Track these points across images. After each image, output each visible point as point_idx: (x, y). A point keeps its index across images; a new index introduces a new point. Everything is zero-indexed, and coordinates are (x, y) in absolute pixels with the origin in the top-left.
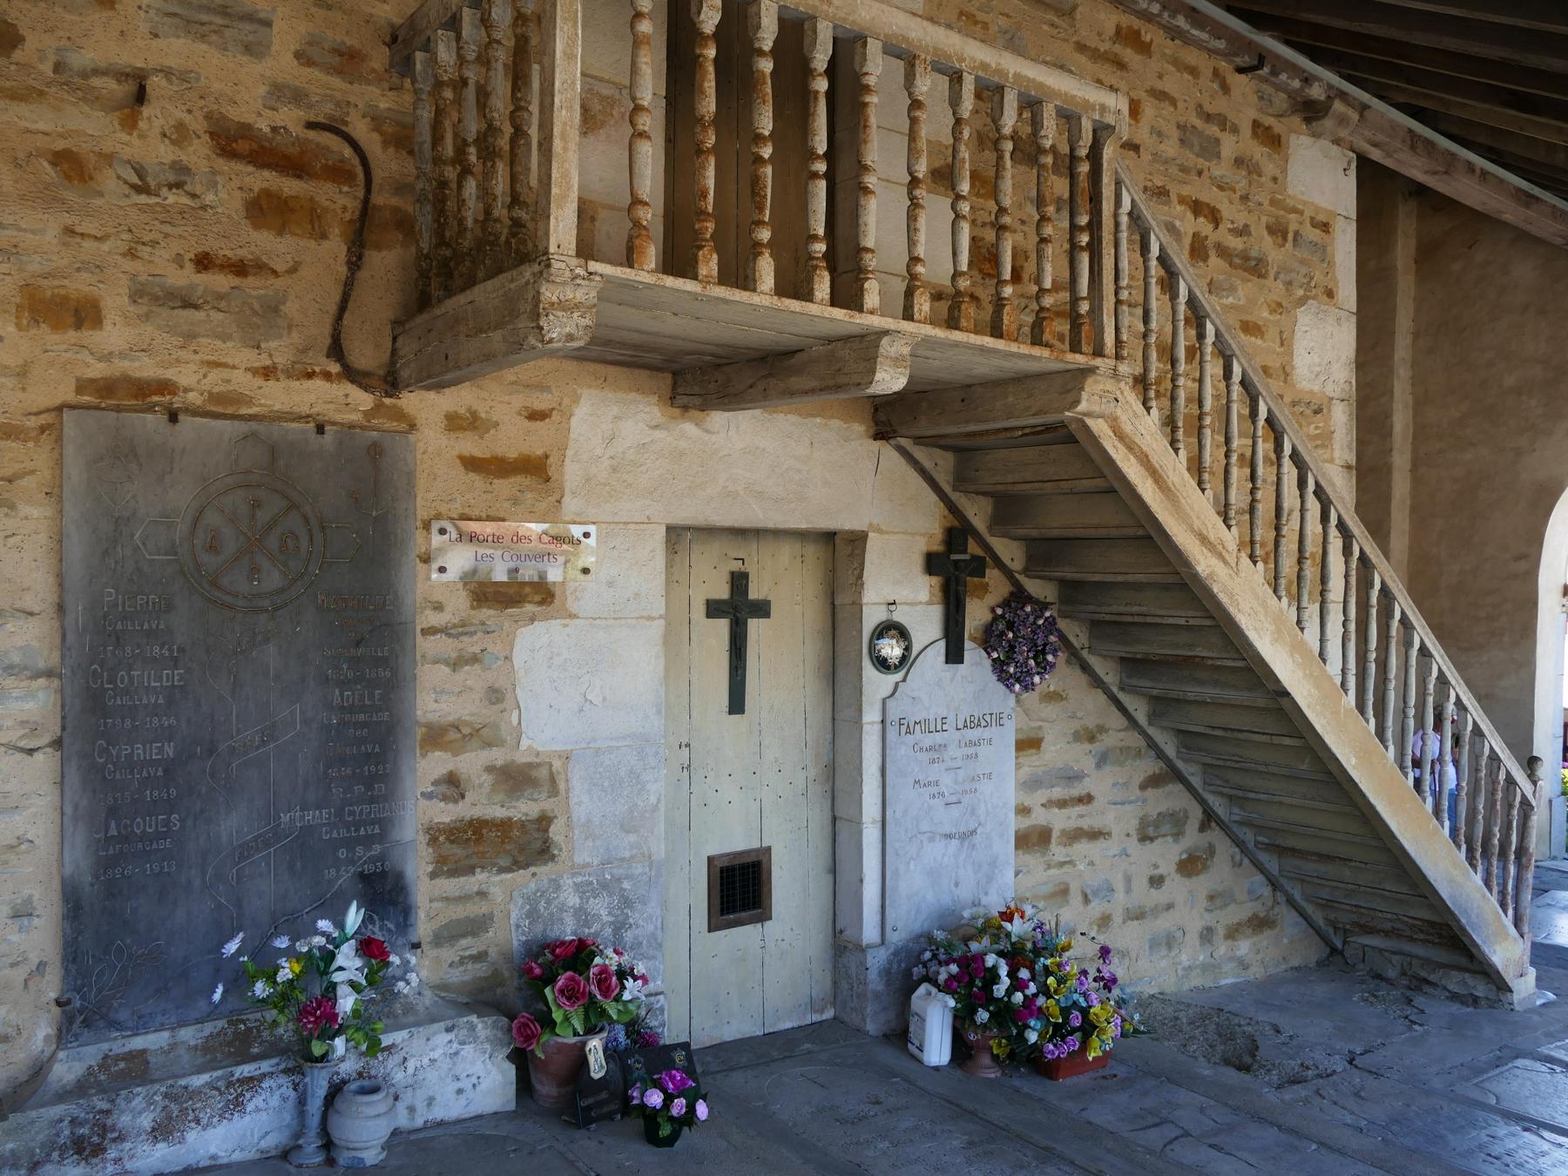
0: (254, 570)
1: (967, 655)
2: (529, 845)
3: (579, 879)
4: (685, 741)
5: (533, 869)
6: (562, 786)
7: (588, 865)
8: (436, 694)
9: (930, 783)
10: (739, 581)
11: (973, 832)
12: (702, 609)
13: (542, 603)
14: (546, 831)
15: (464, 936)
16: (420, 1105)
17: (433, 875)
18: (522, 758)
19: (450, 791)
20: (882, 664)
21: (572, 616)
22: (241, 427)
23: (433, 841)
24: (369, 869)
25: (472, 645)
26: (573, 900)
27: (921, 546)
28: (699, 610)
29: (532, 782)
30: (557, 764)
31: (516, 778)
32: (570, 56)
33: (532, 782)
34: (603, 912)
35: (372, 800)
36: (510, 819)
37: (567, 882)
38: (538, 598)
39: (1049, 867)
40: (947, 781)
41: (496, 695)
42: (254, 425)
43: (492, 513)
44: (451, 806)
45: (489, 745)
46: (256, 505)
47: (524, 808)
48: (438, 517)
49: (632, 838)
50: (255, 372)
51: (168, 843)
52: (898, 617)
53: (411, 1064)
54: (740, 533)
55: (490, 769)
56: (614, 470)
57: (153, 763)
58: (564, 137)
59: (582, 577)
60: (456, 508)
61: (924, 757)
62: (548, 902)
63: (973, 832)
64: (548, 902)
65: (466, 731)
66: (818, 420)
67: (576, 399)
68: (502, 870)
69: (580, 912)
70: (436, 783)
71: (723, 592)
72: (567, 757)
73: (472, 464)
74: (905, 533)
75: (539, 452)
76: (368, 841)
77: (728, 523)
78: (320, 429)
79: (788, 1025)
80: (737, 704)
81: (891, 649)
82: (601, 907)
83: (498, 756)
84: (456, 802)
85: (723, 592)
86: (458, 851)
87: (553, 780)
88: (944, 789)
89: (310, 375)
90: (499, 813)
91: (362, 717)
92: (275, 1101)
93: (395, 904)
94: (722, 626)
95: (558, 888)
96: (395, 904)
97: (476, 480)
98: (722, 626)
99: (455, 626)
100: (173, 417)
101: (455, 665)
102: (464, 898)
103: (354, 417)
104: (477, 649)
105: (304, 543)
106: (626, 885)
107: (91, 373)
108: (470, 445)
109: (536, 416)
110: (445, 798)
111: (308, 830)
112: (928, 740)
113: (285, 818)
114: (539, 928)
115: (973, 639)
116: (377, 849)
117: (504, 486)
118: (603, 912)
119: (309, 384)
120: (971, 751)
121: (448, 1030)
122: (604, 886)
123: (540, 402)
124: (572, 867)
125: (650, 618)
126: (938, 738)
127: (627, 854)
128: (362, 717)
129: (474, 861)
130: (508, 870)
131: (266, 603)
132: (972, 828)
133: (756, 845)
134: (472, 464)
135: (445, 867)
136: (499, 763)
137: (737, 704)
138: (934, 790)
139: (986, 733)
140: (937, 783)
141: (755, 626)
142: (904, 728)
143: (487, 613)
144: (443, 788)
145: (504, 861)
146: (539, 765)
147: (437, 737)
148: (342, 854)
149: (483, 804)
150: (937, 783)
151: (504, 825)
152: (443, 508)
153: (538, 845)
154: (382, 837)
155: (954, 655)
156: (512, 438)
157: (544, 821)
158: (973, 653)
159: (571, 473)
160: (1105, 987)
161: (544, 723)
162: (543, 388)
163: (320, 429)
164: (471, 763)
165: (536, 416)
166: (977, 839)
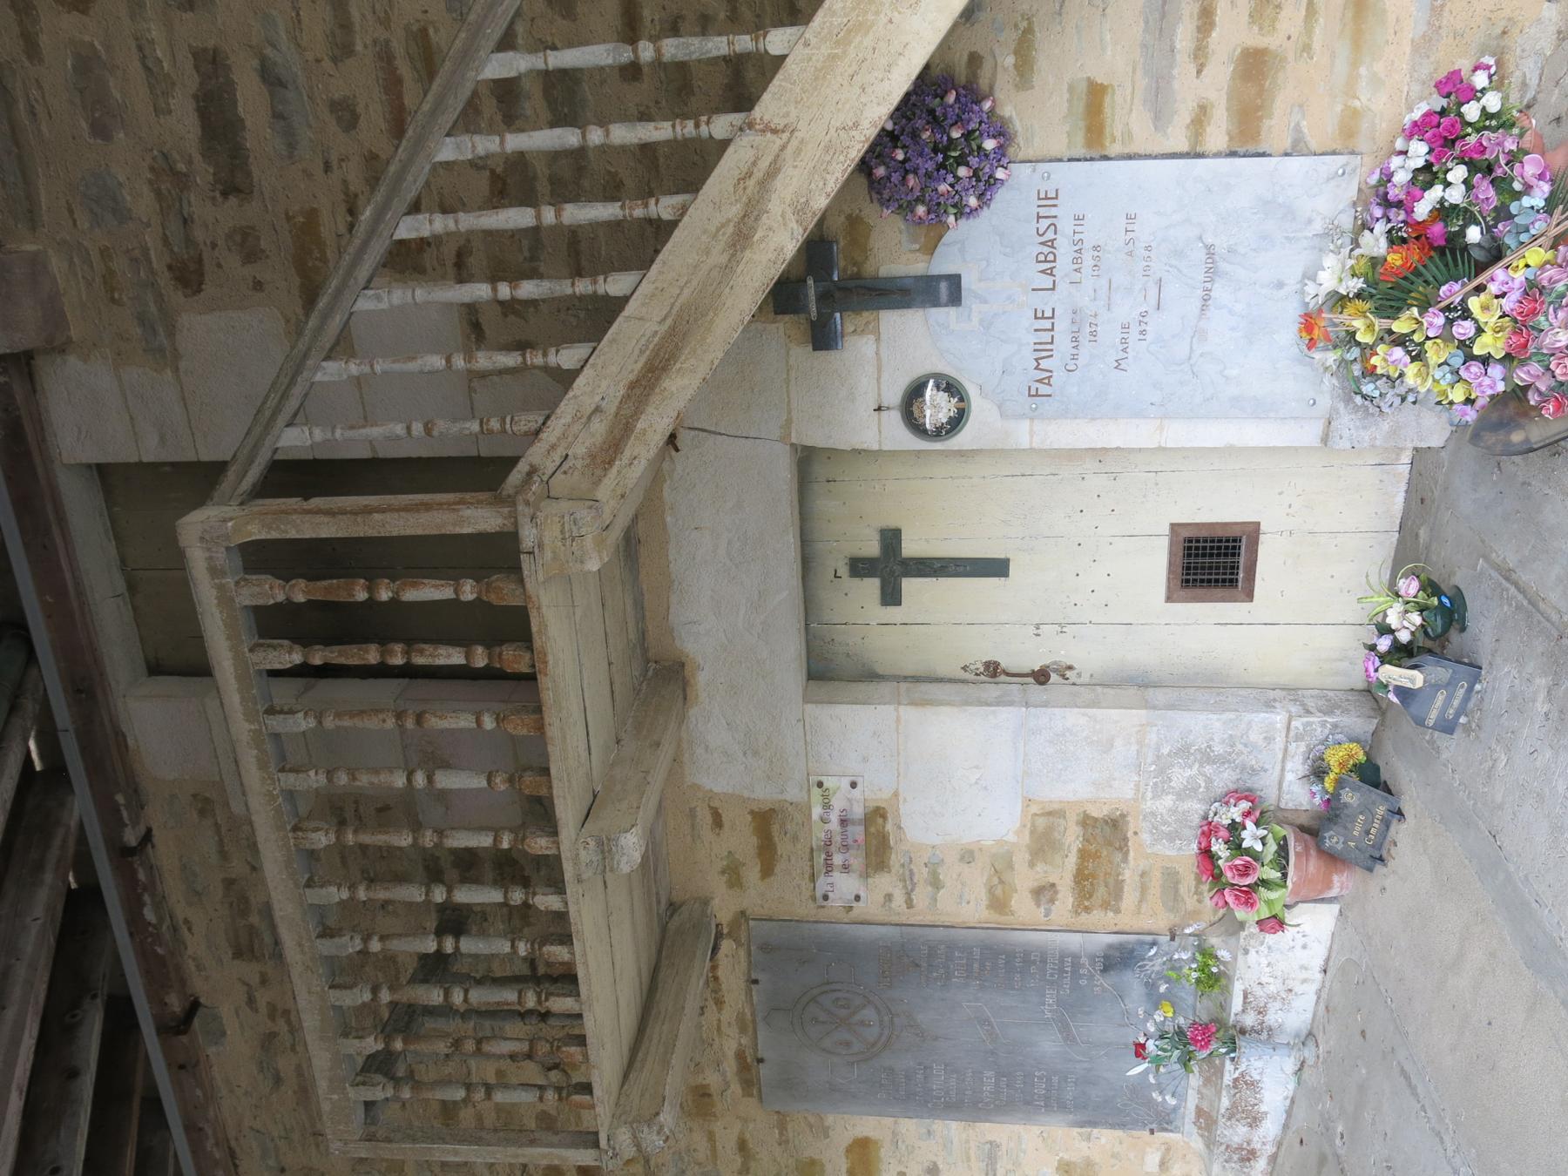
0: (862, 1023)
1: (965, 57)
2: (1107, 832)
3: (1149, 795)
4: (1032, 630)
5: (1130, 834)
6: (1056, 806)
7: (1137, 786)
8: (962, 905)
9: (1124, 341)
10: (860, 567)
11: (1210, 251)
12: (892, 610)
13: (884, 817)
14: (1096, 820)
15: (1177, 890)
16: (1305, 975)
17: (1117, 911)
18: (1026, 838)
19: (1048, 895)
20: (957, 422)
21: (896, 794)
22: (761, 1027)
23: (1087, 910)
24: (1099, 966)
25: (921, 874)
26: (1168, 801)
27: (802, 354)
28: (892, 613)
29: (1049, 830)
30: (1034, 809)
31: (1043, 843)
32: (456, 1153)
33: (1049, 830)
34: (1188, 773)
35: (1044, 961)
36: (1080, 851)
37: (1149, 805)
38: (880, 821)
39: (1307, 48)
40: (1126, 309)
41: (968, 856)
42: (759, 1019)
43: (807, 857)
44: (1059, 896)
45: (1011, 866)
46: (816, 1020)
47: (1072, 838)
48: (814, 898)
49: (1118, 742)
50: (720, 1010)
51: (1055, 1079)
52: (894, 394)
53: (1264, 980)
54: (807, 563)
55: (1032, 865)
56: (756, 753)
57: (997, 1084)
58: (517, 1156)
59: (859, 787)
60: (805, 884)
61: (1086, 349)
62: (1165, 823)
63: (1210, 251)
64: (1165, 823)
65: (995, 880)
66: (668, 519)
67: (696, 787)
68: (1125, 859)
69: (1181, 796)
70: (1038, 906)
71: (872, 585)
72: (1028, 801)
73: (767, 871)
74: (787, 381)
75: (749, 818)
76: (1076, 965)
77: (796, 582)
78: (756, 982)
79: (1400, 499)
80: (997, 568)
81: (936, 407)
82: (1180, 775)
83: (1020, 859)
84: (1056, 892)
85: (872, 585)
86: (1101, 891)
87: (1050, 814)
88: (1135, 314)
89: (716, 978)
90: (1072, 861)
91: (976, 966)
92: (1259, 1064)
93: (1132, 951)
94: (909, 585)
95: (1153, 814)
96: (1132, 951)
97: (779, 868)
98: (909, 585)
99: (905, 887)
100: (760, 1061)
101: (936, 884)
102: (1144, 889)
103: (742, 953)
104: (925, 871)
105: (839, 995)
106: (1165, 751)
107: (739, 1091)
108: (752, 874)
109: (718, 821)
110: (1052, 901)
111: (1059, 1002)
112: (1063, 344)
113: (1049, 1015)
114: (1187, 832)
115: (930, 249)
116: (1084, 960)
117: (783, 847)
118: (1188, 773)
119: (722, 978)
120: (1088, 261)
121: (1246, 952)
122: (1161, 771)
123: (705, 817)
124: (1136, 800)
125: (898, 721)
126: (1062, 325)
127: (1134, 748)
128: (976, 966)
129: (1111, 881)
130: (1126, 854)
131: (886, 1019)
132: (1202, 255)
133: (1164, 543)
134: (767, 871)
135: (1112, 902)
136: (1027, 857)
137: (997, 568)
138: (1134, 334)
139: (1066, 226)
140: (1125, 327)
141: (911, 547)
142: (1043, 389)
143: (895, 860)
144: (1043, 900)
145: (1118, 857)
146: (1033, 825)
147: (998, 903)
148: (1083, 982)
149: (1063, 872)
150: (1125, 327)
151: (1084, 855)
152: (807, 894)
153: (1107, 829)
154: (1076, 957)
155: (949, 290)
156: (740, 840)
157: (1086, 821)
158: (942, 264)
159: (764, 794)
160: (1242, 1160)
161: (996, 821)
162: (692, 813)
163: (756, 982)
164: (1024, 878)
165: (718, 821)
166: (1221, 243)
